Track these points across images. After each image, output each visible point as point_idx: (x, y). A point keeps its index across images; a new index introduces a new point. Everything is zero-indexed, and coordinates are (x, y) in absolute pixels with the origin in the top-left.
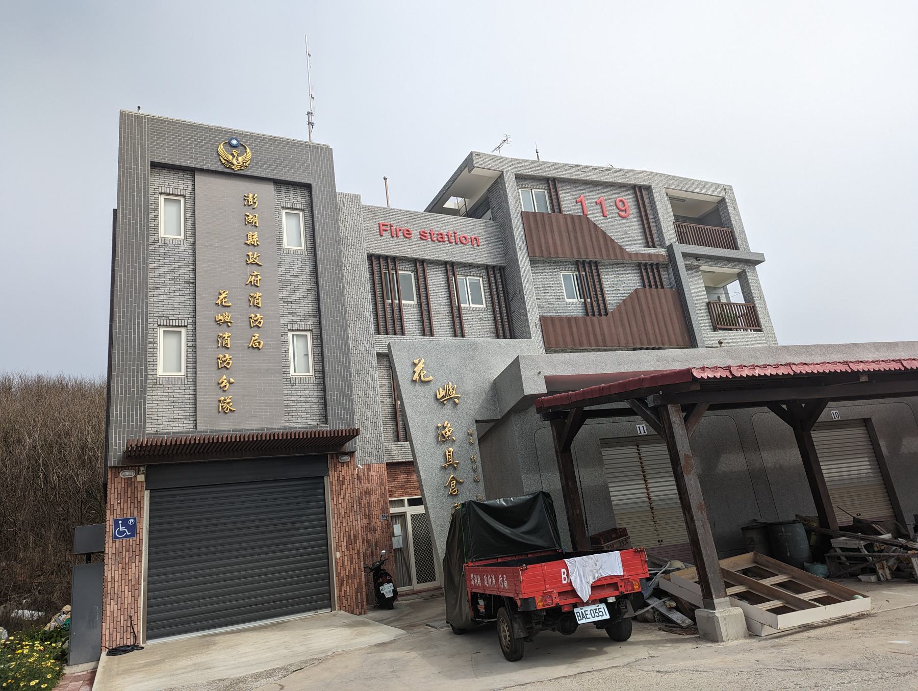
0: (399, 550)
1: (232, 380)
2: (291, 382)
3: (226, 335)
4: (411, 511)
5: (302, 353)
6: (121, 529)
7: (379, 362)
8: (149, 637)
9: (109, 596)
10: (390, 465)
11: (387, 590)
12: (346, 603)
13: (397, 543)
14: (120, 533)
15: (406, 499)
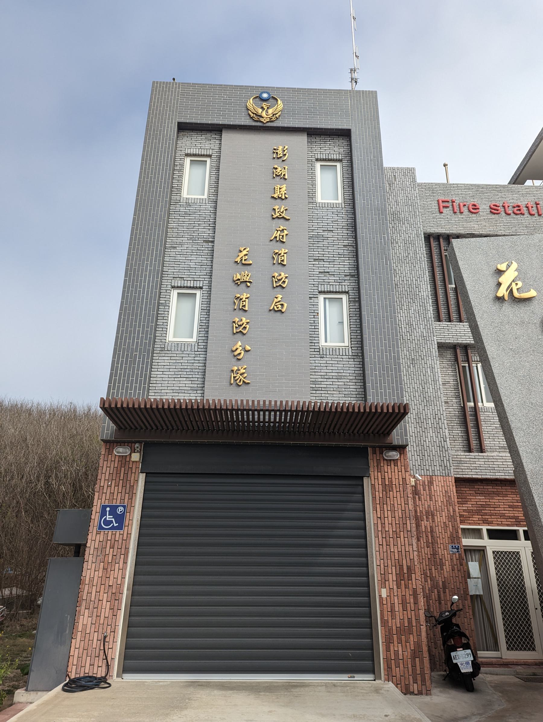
0: (475, 598)
1: (248, 348)
2: (320, 353)
3: (244, 296)
4: (493, 546)
5: (336, 320)
6: (109, 517)
7: (441, 355)
8: (126, 669)
9: (84, 603)
10: (459, 481)
11: (463, 659)
12: (397, 671)
13: (475, 587)
14: (107, 523)
15: (484, 528)
